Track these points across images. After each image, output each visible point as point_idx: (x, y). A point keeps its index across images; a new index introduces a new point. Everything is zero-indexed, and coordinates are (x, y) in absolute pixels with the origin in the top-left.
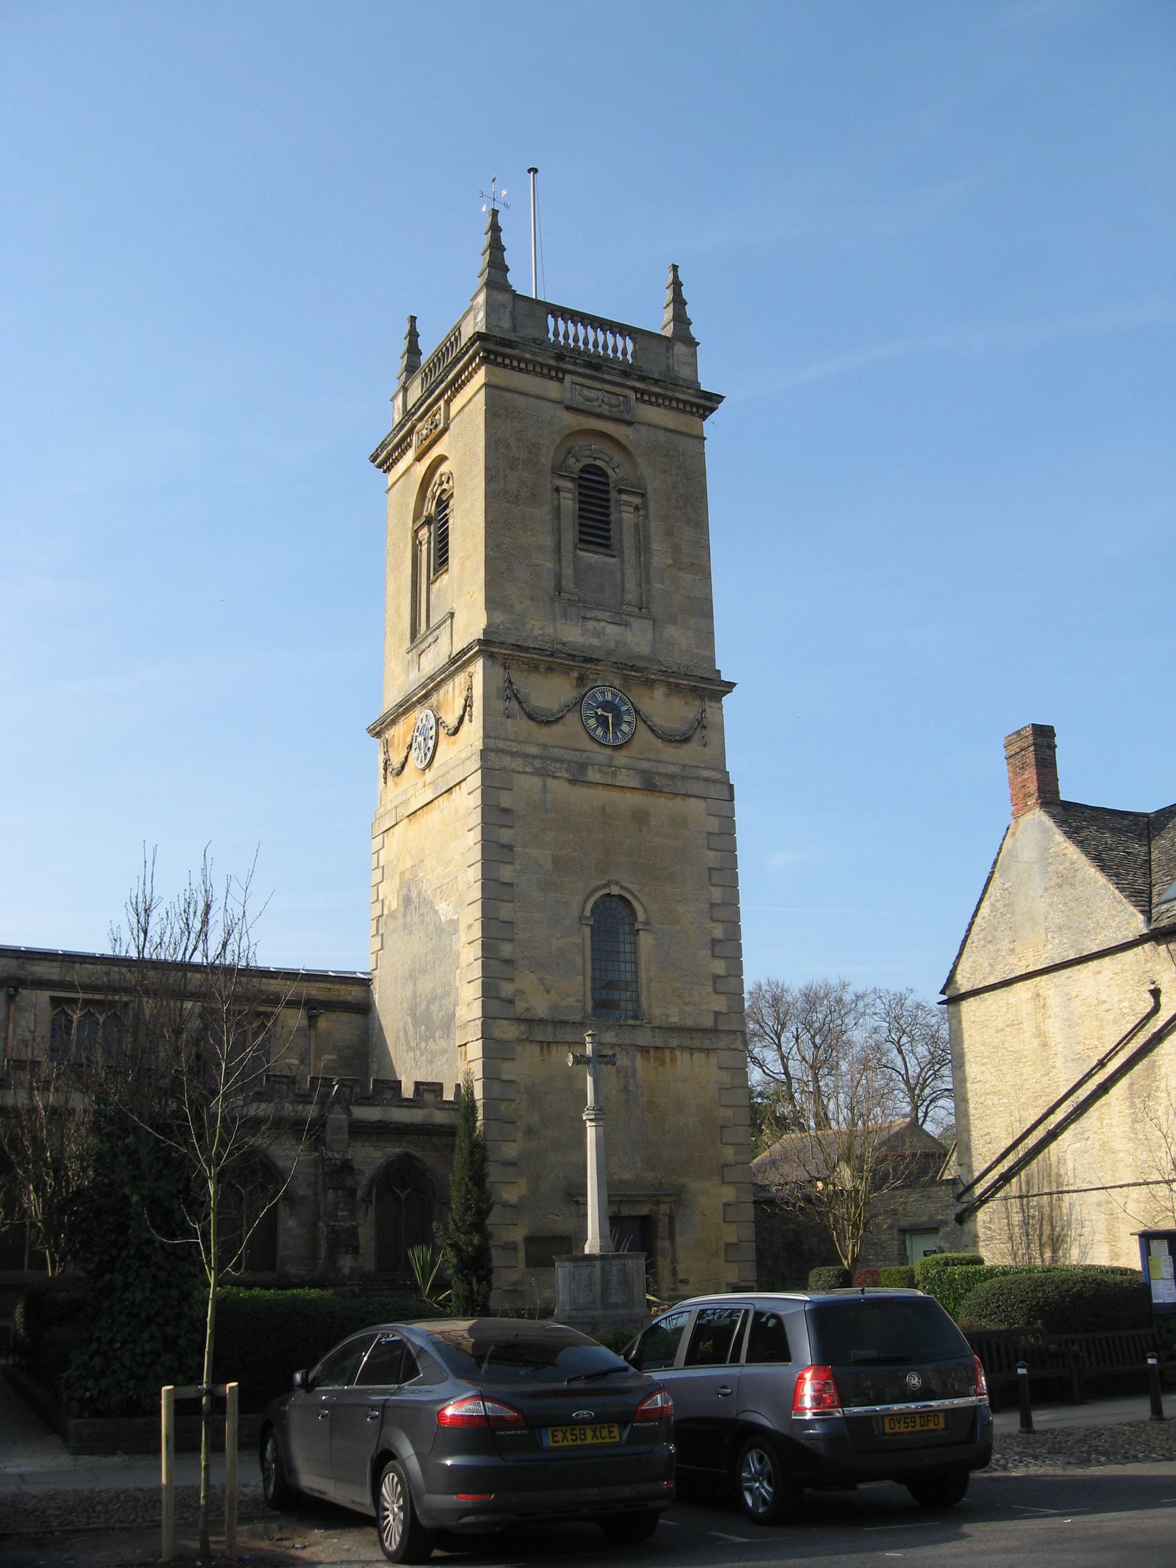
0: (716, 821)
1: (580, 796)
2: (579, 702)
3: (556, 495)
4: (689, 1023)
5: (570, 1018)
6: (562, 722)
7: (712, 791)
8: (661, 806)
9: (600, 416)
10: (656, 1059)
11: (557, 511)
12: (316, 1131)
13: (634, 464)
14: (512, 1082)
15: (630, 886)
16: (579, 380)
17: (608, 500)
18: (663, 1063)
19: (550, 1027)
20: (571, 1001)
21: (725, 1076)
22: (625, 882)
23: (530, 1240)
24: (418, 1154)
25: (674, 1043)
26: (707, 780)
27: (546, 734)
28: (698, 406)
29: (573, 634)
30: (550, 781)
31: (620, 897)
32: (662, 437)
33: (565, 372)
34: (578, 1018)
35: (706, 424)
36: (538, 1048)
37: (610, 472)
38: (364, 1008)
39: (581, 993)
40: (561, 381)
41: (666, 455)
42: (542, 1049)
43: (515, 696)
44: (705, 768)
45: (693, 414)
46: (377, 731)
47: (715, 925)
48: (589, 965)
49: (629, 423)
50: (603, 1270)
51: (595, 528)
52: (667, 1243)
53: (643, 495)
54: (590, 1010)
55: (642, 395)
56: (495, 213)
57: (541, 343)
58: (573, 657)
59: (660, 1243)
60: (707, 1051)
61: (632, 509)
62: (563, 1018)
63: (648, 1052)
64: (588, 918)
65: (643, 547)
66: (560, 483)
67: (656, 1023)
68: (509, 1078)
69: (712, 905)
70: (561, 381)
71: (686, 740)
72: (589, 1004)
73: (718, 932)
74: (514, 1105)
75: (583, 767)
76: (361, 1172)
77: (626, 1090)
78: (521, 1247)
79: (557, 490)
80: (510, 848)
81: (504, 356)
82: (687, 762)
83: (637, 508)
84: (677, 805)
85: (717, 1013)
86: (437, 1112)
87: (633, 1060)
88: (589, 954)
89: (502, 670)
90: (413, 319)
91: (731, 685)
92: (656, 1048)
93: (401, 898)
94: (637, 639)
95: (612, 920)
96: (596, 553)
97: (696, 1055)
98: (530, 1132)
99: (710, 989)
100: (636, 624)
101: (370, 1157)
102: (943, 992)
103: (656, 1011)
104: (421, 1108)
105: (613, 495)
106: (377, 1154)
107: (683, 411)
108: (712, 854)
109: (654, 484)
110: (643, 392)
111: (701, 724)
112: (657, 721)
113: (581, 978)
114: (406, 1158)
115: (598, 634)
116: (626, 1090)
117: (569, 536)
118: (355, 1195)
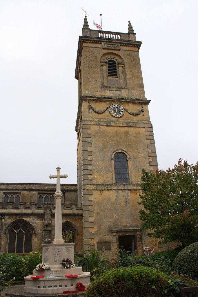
1: (109, 129)
2: (108, 108)
5: (109, 184)
6: (104, 113)
8: (132, 130)
10: (134, 193)
16: (105, 43)
17: (116, 67)
19: (103, 186)
20: (109, 179)
22: (123, 148)
23: (98, 243)
24: (71, 221)
26: (145, 123)
27: (100, 116)
29: (107, 94)
30: (101, 127)
31: (122, 152)
32: (128, 52)
34: (111, 184)
37: (115, 61)
38: (76, 191)
39: (112, 177)
40: (101, 44)
41: (129, 56)
42: (101, 192)
43: (91, 108)
44: (144, 121)
47: (150, 158)
48: (114, 170)
49: (119, 50)
53: (124, 64)
56: (86, 16)
59: (138, 243)
63: (132, 191)
65: (125, 74)
67: (134, 183)
68: (91, 200)
71: (138, 114)
72: (114, 179)
73: (151, 159)
74: (93, 207)
75: (110, 122)
78: (96, 245)
79: (102, 65)
80: (90, 143)
83: (123, 67)
84: (137, 130)
86: (76, 210)
87: (128, 193)
88: (113, 167)
90: (129, 21)
91: (150, 101)
92: (134, 190)
94: (124, 94)
95: (121, 158)
96: (113, 77)
98: (98, 213)
104: (71, 209)
105: (117, 66)
108: (147, 140)
110: (122, 43)
111: (142, 111)
112: (130, 111)
115: (113, 93)
117: (106, 74)
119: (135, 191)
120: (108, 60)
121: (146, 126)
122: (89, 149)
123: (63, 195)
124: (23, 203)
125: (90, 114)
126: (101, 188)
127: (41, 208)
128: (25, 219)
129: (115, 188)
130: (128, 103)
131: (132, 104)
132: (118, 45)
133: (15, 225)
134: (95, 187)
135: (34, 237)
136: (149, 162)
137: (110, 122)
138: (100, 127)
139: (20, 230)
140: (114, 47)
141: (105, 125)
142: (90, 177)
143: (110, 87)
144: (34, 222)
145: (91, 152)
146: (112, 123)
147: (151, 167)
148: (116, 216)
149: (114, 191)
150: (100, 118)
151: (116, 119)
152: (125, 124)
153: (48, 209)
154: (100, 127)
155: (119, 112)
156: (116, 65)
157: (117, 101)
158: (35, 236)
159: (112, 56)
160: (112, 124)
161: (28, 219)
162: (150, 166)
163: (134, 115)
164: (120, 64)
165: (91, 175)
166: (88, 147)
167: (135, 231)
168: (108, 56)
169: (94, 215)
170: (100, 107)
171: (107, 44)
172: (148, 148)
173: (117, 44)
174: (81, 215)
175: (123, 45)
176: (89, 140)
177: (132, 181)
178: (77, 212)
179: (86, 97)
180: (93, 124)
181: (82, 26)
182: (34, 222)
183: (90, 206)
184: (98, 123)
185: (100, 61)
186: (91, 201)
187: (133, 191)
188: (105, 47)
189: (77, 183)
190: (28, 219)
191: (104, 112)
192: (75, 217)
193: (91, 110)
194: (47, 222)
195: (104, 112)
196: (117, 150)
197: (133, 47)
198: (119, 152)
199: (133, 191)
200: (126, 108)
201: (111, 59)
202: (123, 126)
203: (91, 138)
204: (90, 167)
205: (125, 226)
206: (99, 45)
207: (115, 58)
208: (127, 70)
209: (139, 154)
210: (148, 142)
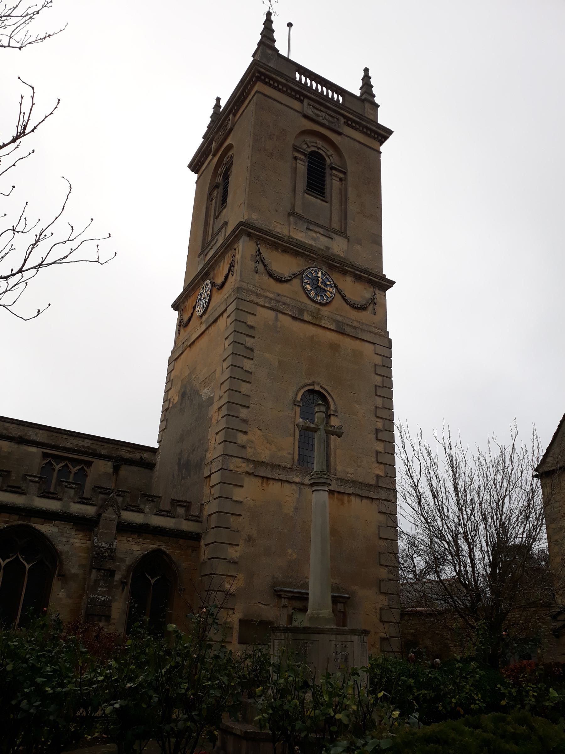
1: (297, 326)
2: (301, 273)
3: (294, 161)
5: (283, 464)
8: (347, 342)
11: (295, 170)
12: (85, 525)
14: (239, 502)
15: (326, 387)
16: (311, 103)
17: (324, 173)
18: (343, 503)
19: (269, 468)
21: (382, 518)
22: (322, 382)
24: (168, 551)
25: (350, 491)
26: (375, 334)
30: (280, 316)
32: (357, 145)
34: (289, 465)
35: (381, 147)
36: (260, 481)
37: (327, 158)
38: (150, 466)
40: (302, 102)
43: (262, 261)
45: (375, 138)
47: (378, 420)
49: (340, 134)
51: (316, 183)
53: (345, 173)
54: (296, 461)
55: (348, 121)
56: (269, 14)
61: (338, 180)
62: (279, 463)
63: (333, 494)
64: (299, 402)
65: (344, 200)
66: (297, 154)
67: (339, 475)
68: (238, 499)
69: (376, 407)
71: (364, 308)
73: (380, 425)
75: (301, 311)
76: (123, 560)
79: (296, 158)
82: (364, 321)
83: (341, 180)
85: (378, 476)
86: (185, 522)
89: (255, 245)
90: (366, 70)
91: (391, 283)
92: (339, 493)
93: (181, 394)
94: (338, 247)
97: (365, 501)
99: (374, 460)
101: (132, 549)
105: (328, 171)
106: (137, 548)
112: (348, 295)
113: (292, 439)
114: (157, 553)
115: (314, 239)
117: (302, 185)
118: (114, 576)
119: (340, 496)
120: (292, 166)
121: (377, 340)
122: (248, 365)
123: (113, 473)
124: (37, 479)
125: (257, 275)
126: (265, 471)
127: (91, 502)
128: (38, 527)
129: (297, 480)
130: (344, 273)
131: (354, 279)
132: (338, 119)
134: (250, 468)
135: (56, 584)
136: (377, 431)
137: (301, 311)
138: (277, 317)
139: (17, 556)
140: (329, 121)
141: (291, 316)
142: (242, 439)
143: (309, 222)
144: (64, 539)
145: (251, 373)
146: (305, 314)
147: (378, 443)
149: (294, 486)
150: (279, 292)
151: (314, 305)
152: (334, 324)
153: (112, 506)
154: (277, 317)
156: (324, 169)
157: (324, 261)
158: (60, 583)
159: (320, 143)
160: (307, 317)
161: (45, 528)
162: (378, 439)
163: (354, 307)
164: (336, 169)
165: (245, 433)
166: (246, 360)
168: (313, 139)
169: (241, 542)
170: (284, 264)
171: (314, 107)
172: (377, 395)
173: (339, 116)
174: (197, 537)
175: (350, 123)
176: (249, 342)
177: (335, 469)
178: (186, 526)
179: (253, 228)
180: (262, 303)
182: (64, 539)
183: (235, 517)
184: (273, 304)
185: (294, 145)
186: (237, 502)
187: (336, 494)
188: (309, 112)
189: (156, 446)
190: (45, 528)
191: (290, 280)
192: (181, 541)
193: (261, 267)
194: (104, 545)
195: (290, 280)
196: (310, 384)
197: (369, 136)
198: (312, 391)
199: (336, 494)
200: (340, 287)
201: (316, 150)
202: (329, 327)
203: (253, 337)
204: (244, 413)
206: (296, 102)
207: (328, 150)
208: (350, 190)
209: (357, 406)
210: (378, 380)
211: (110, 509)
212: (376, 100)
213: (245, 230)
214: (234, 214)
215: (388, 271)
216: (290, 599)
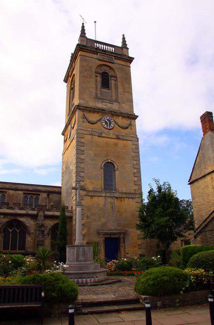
0: (134, 146)
2: (101, 119)
4: (128, 192)
7: (133, 139)
8: (121, 143)
9: (106, 61)
12: (34, 217)
13: (115, 72)
20: (98, 186)
25: (124, 196)
28: (129, 60)
29: (100, 105)
30: (94, 137)
32: (120, 66)
33: (98, 52)
38: (60, 193)
40: (97, 54)
46: (63, 134)
49: (113, 63)
50: (77, 250)
51: (105, 83)
52: (123, 244)
53: (116, 78)
56: (83, 24)
57: (93, 48)
58: (99, 109)
59: (121, 244)
60: (133, 198)
65: (117, 88)
66: (97, 75)
70: (97, 54)
71: (127, 128)
73: (135, 171)
75: (101, 133)
77: (112, 207)
79: (96, 76)
81: (84, 49)
83: (115, 80)
88: (103, 175)
90: (123, 35)
94: (115, 107)
95: (109, 168)
97: (130, 199)
100: (115, 103)
101: (50, 223)
102: (189, 181)
103: (120, 189)
107: (125, 61)
109: (119, 75)
111: (130, 125)
116: (112, 207)
117: (99, 86)
120: (101, 71)
121: (133, 139)
122: (82, 157)
128: (20, 219)
129: (104, 195)
130: (118, 116)
133: (10, 224)
135: (27, 236)
148: (103, 220)
155: (110, 124)
161: (22, 219)
163: (123, 128)
167: (120, 234)
170: (94, 117)
181: (122, 41)
200: (116, 121)
204: (82, 174)
205: (111, 230)
208: (119, 83)
211: (41, 211)
212: (128, 46)
213: (79, 107)
214: (76, 102)
215: (136, 112)
216: (104, 235)
